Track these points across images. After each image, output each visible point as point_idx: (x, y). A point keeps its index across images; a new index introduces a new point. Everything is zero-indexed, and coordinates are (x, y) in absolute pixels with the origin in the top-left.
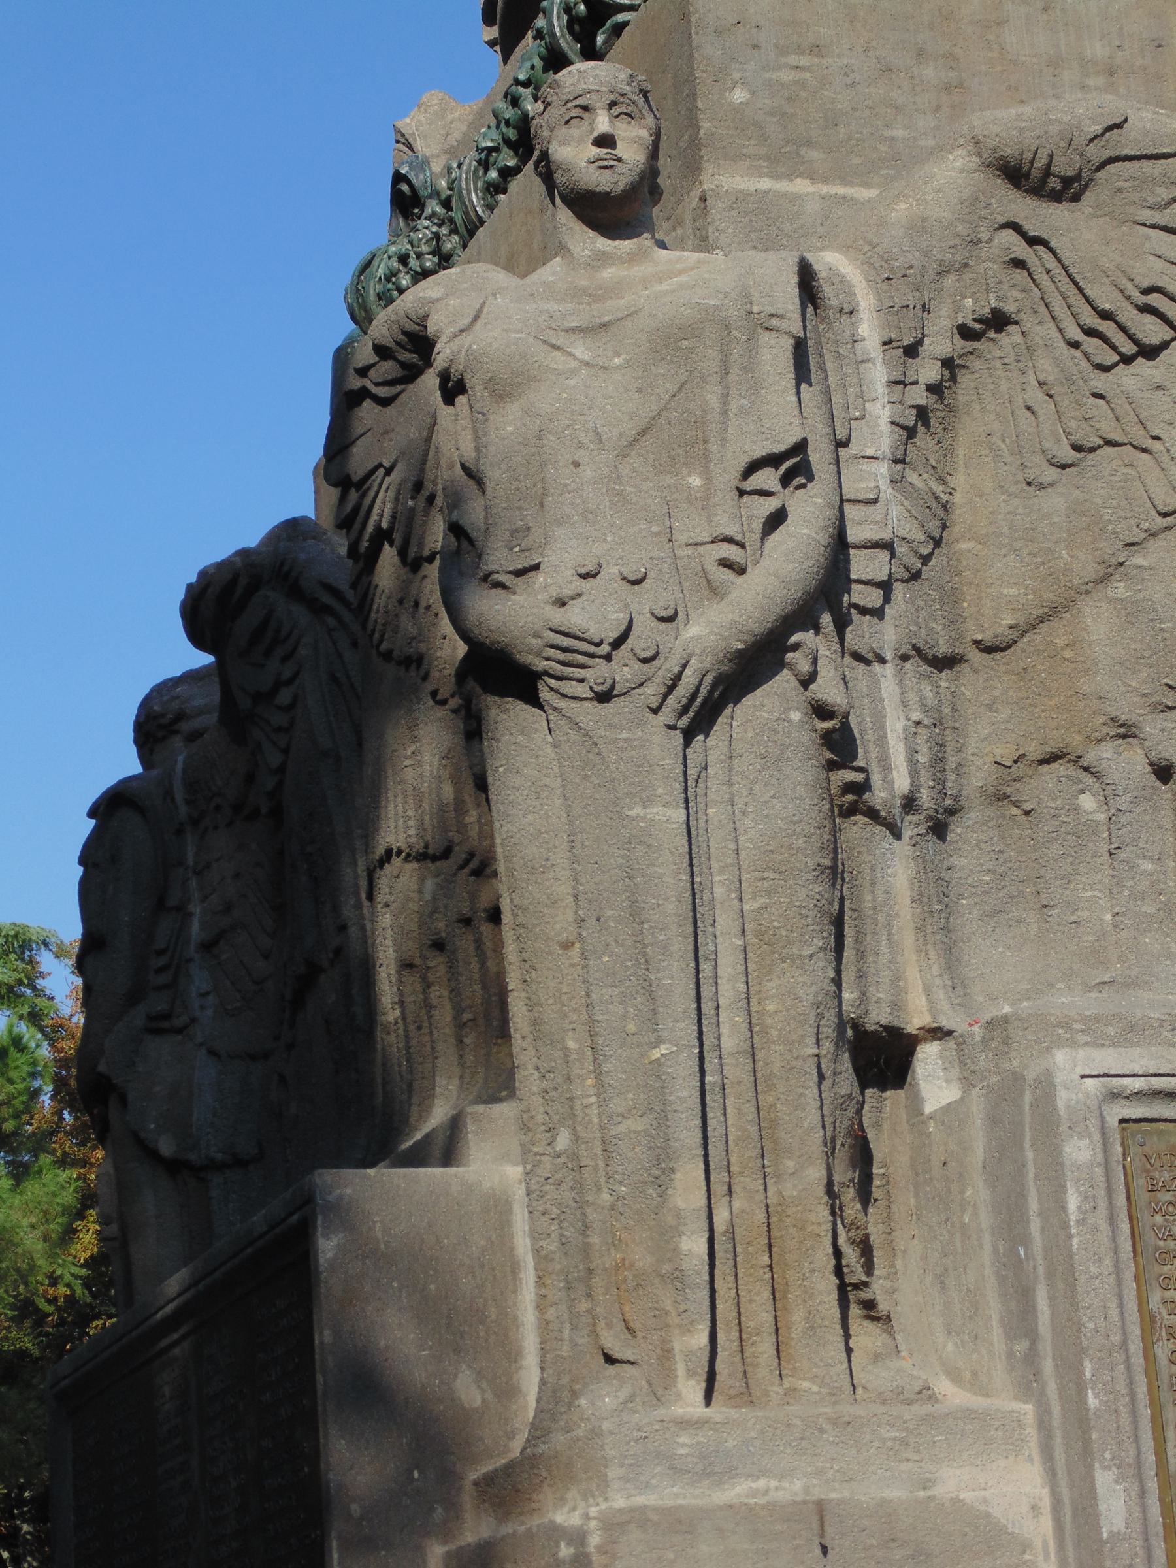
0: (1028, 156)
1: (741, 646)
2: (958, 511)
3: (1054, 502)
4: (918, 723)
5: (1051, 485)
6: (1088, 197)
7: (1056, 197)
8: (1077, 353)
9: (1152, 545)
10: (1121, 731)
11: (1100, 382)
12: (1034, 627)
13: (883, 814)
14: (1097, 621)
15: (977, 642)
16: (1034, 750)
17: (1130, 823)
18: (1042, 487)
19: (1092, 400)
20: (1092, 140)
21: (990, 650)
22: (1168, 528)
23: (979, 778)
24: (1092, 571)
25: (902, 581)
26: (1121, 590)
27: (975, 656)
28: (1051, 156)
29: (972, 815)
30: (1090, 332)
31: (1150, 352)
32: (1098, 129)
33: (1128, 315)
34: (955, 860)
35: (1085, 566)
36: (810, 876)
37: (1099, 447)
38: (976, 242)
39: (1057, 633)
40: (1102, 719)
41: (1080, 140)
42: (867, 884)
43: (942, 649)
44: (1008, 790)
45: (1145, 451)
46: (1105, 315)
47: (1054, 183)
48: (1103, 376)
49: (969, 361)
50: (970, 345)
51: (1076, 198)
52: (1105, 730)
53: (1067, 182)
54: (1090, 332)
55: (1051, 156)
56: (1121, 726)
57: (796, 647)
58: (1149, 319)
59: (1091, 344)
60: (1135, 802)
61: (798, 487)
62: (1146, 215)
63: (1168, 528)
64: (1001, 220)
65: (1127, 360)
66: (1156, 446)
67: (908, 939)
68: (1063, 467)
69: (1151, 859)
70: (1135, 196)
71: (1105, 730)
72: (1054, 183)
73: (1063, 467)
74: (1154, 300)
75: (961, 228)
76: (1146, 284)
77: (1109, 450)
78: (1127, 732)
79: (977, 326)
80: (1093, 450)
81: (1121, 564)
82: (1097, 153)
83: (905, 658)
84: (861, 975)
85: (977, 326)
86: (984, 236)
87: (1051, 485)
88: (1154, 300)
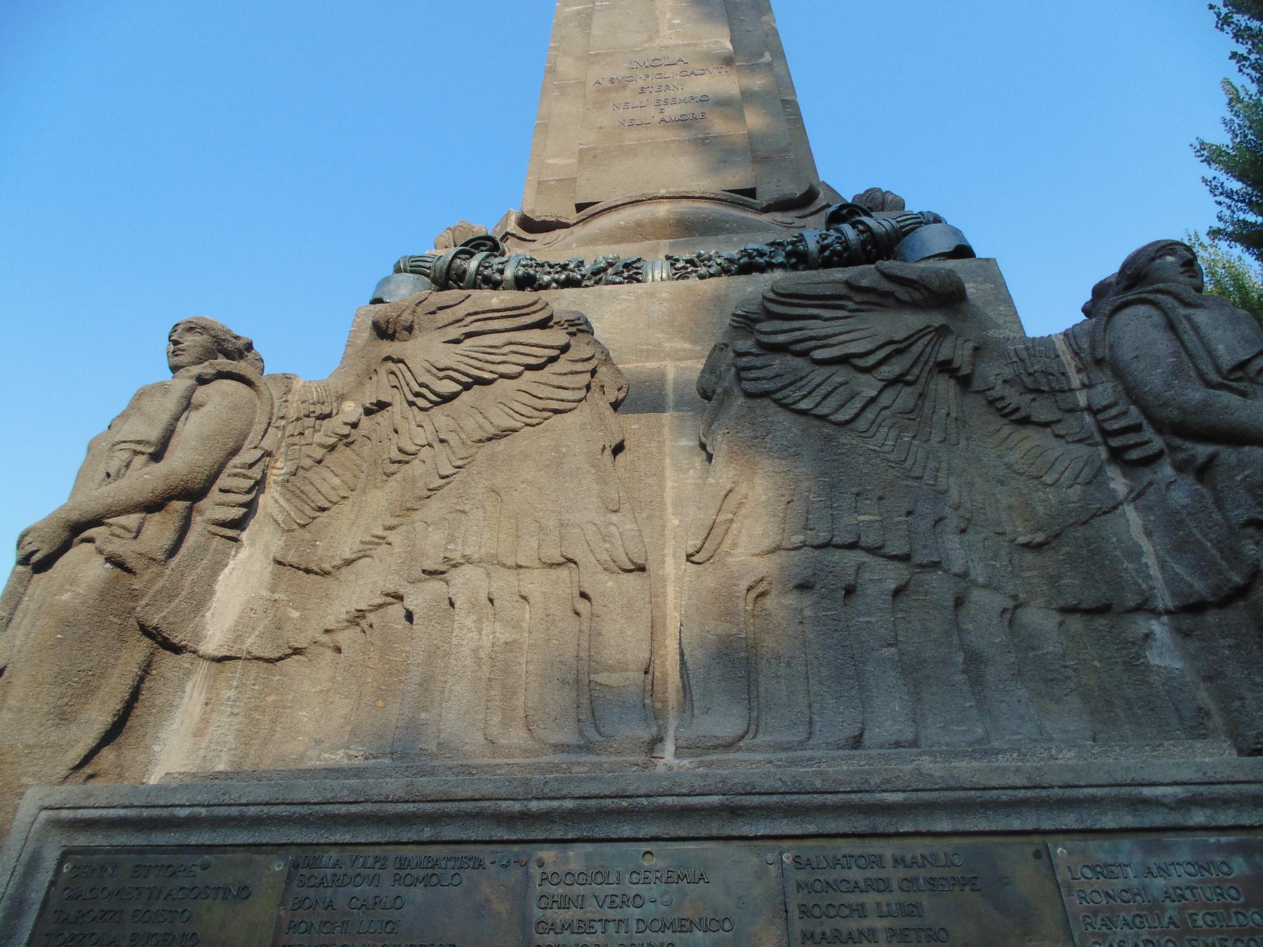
30: (417, 395)
31: (447, 398)
64: (384, 356)
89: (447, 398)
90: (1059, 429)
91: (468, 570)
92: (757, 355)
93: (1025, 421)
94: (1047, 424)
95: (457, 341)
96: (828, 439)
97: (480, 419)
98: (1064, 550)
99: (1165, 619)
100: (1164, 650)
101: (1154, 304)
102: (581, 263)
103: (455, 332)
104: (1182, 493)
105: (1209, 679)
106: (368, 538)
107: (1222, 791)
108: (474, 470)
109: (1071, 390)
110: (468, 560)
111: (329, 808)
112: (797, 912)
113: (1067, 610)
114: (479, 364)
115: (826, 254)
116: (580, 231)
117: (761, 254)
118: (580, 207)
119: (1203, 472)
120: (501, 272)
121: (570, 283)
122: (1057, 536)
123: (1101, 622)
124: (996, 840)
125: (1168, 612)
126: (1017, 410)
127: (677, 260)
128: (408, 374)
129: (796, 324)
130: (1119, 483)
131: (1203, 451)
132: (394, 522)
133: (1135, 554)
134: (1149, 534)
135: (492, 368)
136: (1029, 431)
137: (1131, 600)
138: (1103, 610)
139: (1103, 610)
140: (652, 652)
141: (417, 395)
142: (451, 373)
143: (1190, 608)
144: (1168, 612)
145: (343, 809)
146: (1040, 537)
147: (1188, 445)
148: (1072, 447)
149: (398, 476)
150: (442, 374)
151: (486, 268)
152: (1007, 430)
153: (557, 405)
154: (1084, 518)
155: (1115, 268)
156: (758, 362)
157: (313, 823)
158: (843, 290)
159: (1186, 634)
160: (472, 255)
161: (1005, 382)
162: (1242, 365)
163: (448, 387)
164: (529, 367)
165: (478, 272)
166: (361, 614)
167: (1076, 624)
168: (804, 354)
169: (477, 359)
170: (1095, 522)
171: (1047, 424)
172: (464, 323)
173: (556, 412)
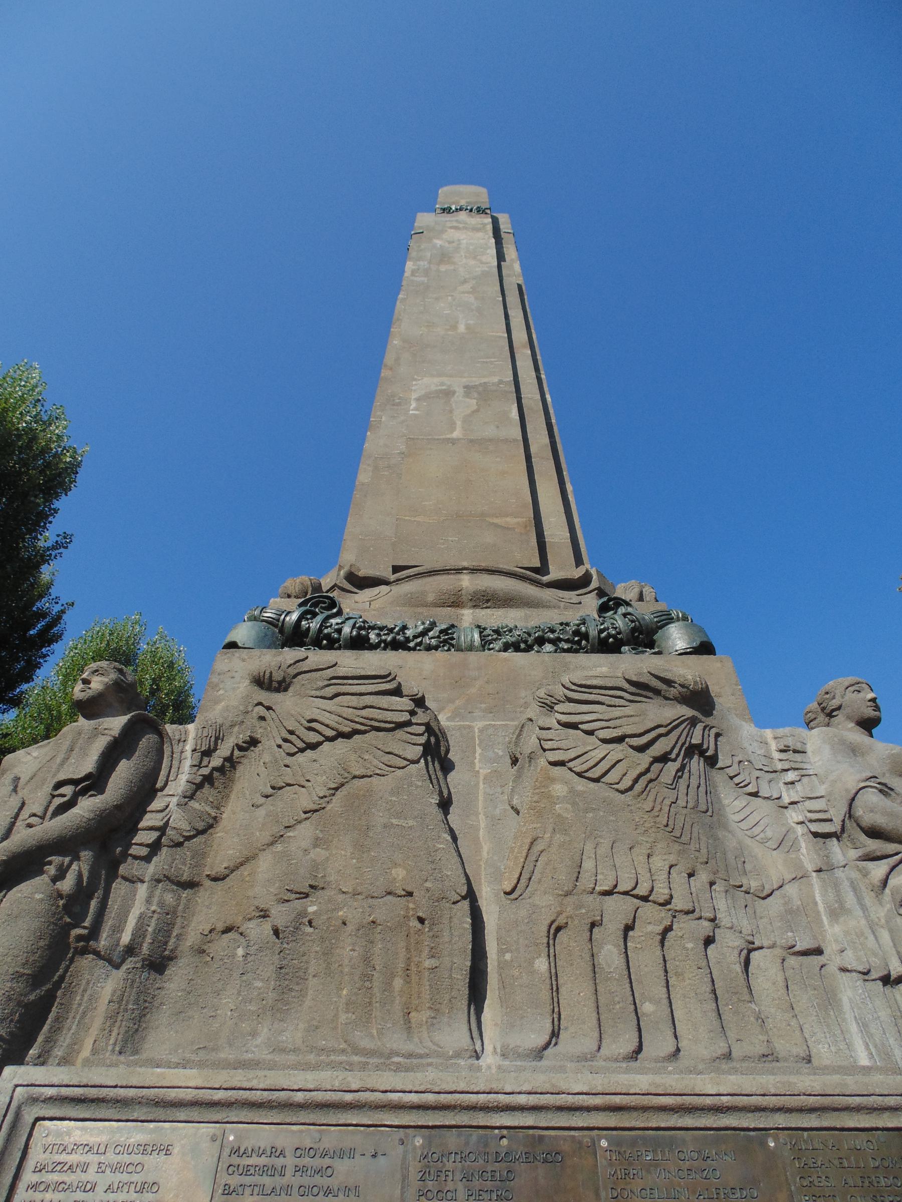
0: (262, 674)
1: (5, 858)
2: (624, 922)
3: (261, 812)
4: (154, 912)
5: (261, 805)
6: (291, 689)
7: (278, 690)
8: (281, 750)
9: (298, 827)
10: (262, 913)
11: (289, 760)
12: (238, 868)
13: (103, 953)
14: (265, 864)
15: (208, 876)
16: (220, 926)
17: (254, 961)
18: (258, 807)
19: (284, 768)
20: (289, 666)
21: (215, 879)
22: (306, 819)
23: (192, 938)
24: (268, 839)
25: (169, 846)
26: (279, 847)
27: (208, 883)
28: (271, 673)
29: (182, 960)
30: (286, 740)
31: (313, 746)
32: (292, 662)
33: (302, 732)
34: (166, 985)
35: (266, 837)
36: (8, 977)
37: (283, 787)
38: (247, 712)
39: (245, 871)
40: (253, 908)
41: (284, 667)
42: (80, 991)
43: (185, 877)
44: (205, 947)
45: (303, 787)
46: (291, 732)
47: (275, 684)
48: (291, 758)
49: (242, 760)
50: (242, 753)
51: (286, 690)
52: (254, 913)
53: (280, 683)
54: (286, 740)
55: (271, 673)
56: (261, 911)
57: (50, 863)
58: (312, 733)
59: (286, 745)
60: (260, 950)
61: (91, 796)
62: (314, 693)
63: (306, 819)
64: (256, 702)
65: (302, 750)
66: (309, 784)
67: (97, 1021)
68: (267, 797)
69: (262, 980)
70: (309, 686)
71: (254, 913)
72: (275, 684)
73: (267, 797)
74: (313, 725)
75: (241, 708)
76: (308, 718)
77: (288, 788)
78: (264, 914)
79: (244, 745)
80: (280, 788)
81: (282, 836)
82: (292, 671)
83: (159, 881)
84: (47, 1040)
85: (244, 745)
86: (250, 710)
87: (261, 805)
88: (313, 725)
90: (767, 844)
102: (404, 628)
107: (372, 1098)
115: (603, 635)
116: (397, 590)
117: (552, 631)
118: (396, 569)
120: (339, 631)
121: (395, 645)
127: (485, 629)
129: (585, 708)
140: (669, 873)
151: (327, 627)
157: (276, 1107)
160: (315, 615)
163: (313, 738)
165: (320, 630)
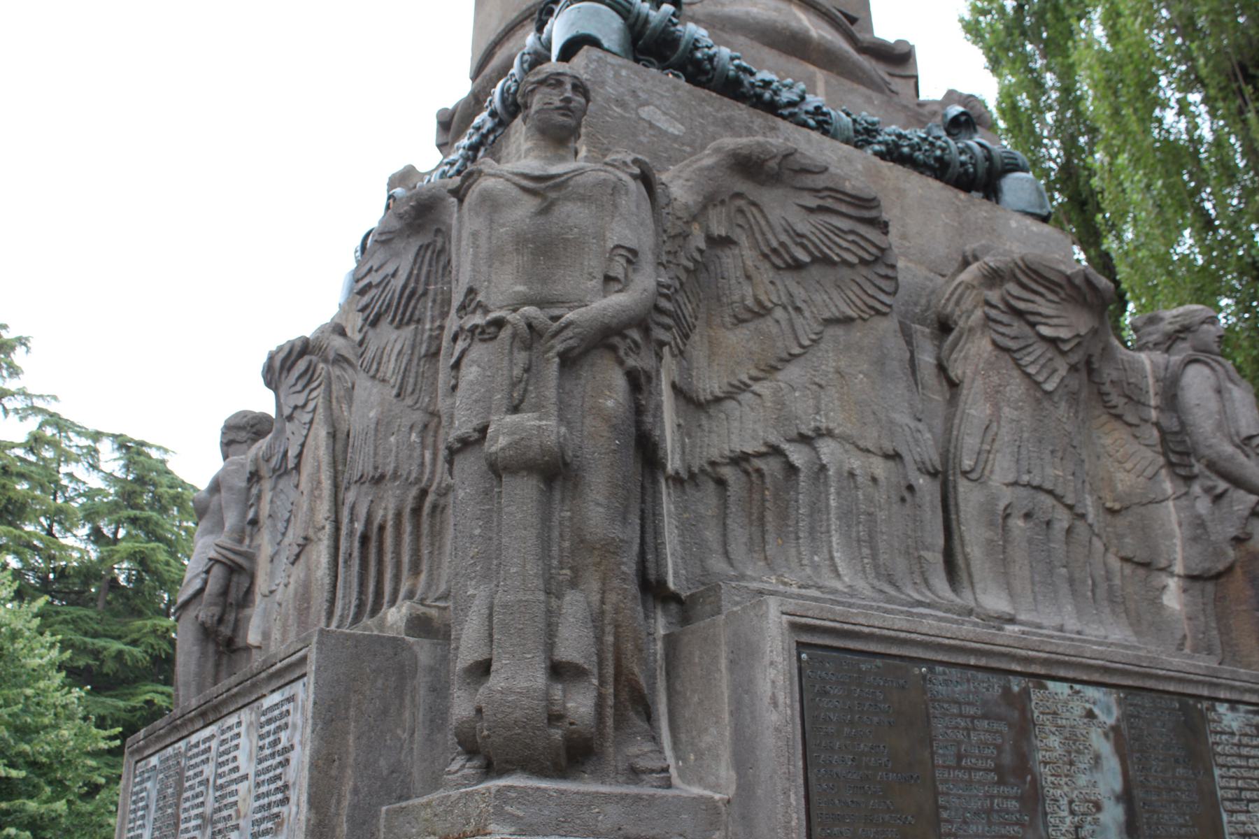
31: (797, 266)
89: (797, 266)
91: (829, 441)
92: (1003, 312)
93: (1119, 417)
94: (1130, 425)
95: (810, 210)
96: (1038, 401)
97: (825, 297)
98: (1129, 519)
99: (1176, 579)
100: (1173, 598)
101: (1212, 369)
103: (813, 202)
104: (1203, 506)
105: (1190, 619)
106: (736, 383)
108: (822, 346)
109: (1149, 406)
110: (829, 433)
111: (940, 640)
112: (180, 669)
113: (1125, 560)
114: (828, 243)
119: (1218, 498)
122: (1127, 508)
123: (1141, 572)
124: (897, 662)
125: (1179, 576)
126: (1115, 407)
128: (763, 223)
130: (1168, 487)
131: (1222, 485)
132: (761, 375)
133: (1171, 536)
134: (1180, 525)
135: (837, 250)
136: (1118, 424)
137: (1163, 563)
138: (1146, 565)
139: (1146, 565)
141: (774, 251)
142: (805, 242)
143: (1191, 578)
144: (1179, 576)
145: (946, 641)
146: (1117, 506)
147: (1214, 477)
148: (1143, 448)
149: (751, 326)
150: (798, 240)
152: (1105, 418)
153: (879, 306)
154: (1144, 501)
155: (328, 321)
156: (1001, 317)
158: (1064, 282)
159: (1185, 591)
161: (1112, 382)
162: (1250, 438)
164: (863, 262)
166: (745, 457)
167: (1128, 569)
168: (1033, 325)
169: (826, 236)
170: (1150, 506)
171: (1130, 425)
172: (821, 194)
173: (878, 312)
